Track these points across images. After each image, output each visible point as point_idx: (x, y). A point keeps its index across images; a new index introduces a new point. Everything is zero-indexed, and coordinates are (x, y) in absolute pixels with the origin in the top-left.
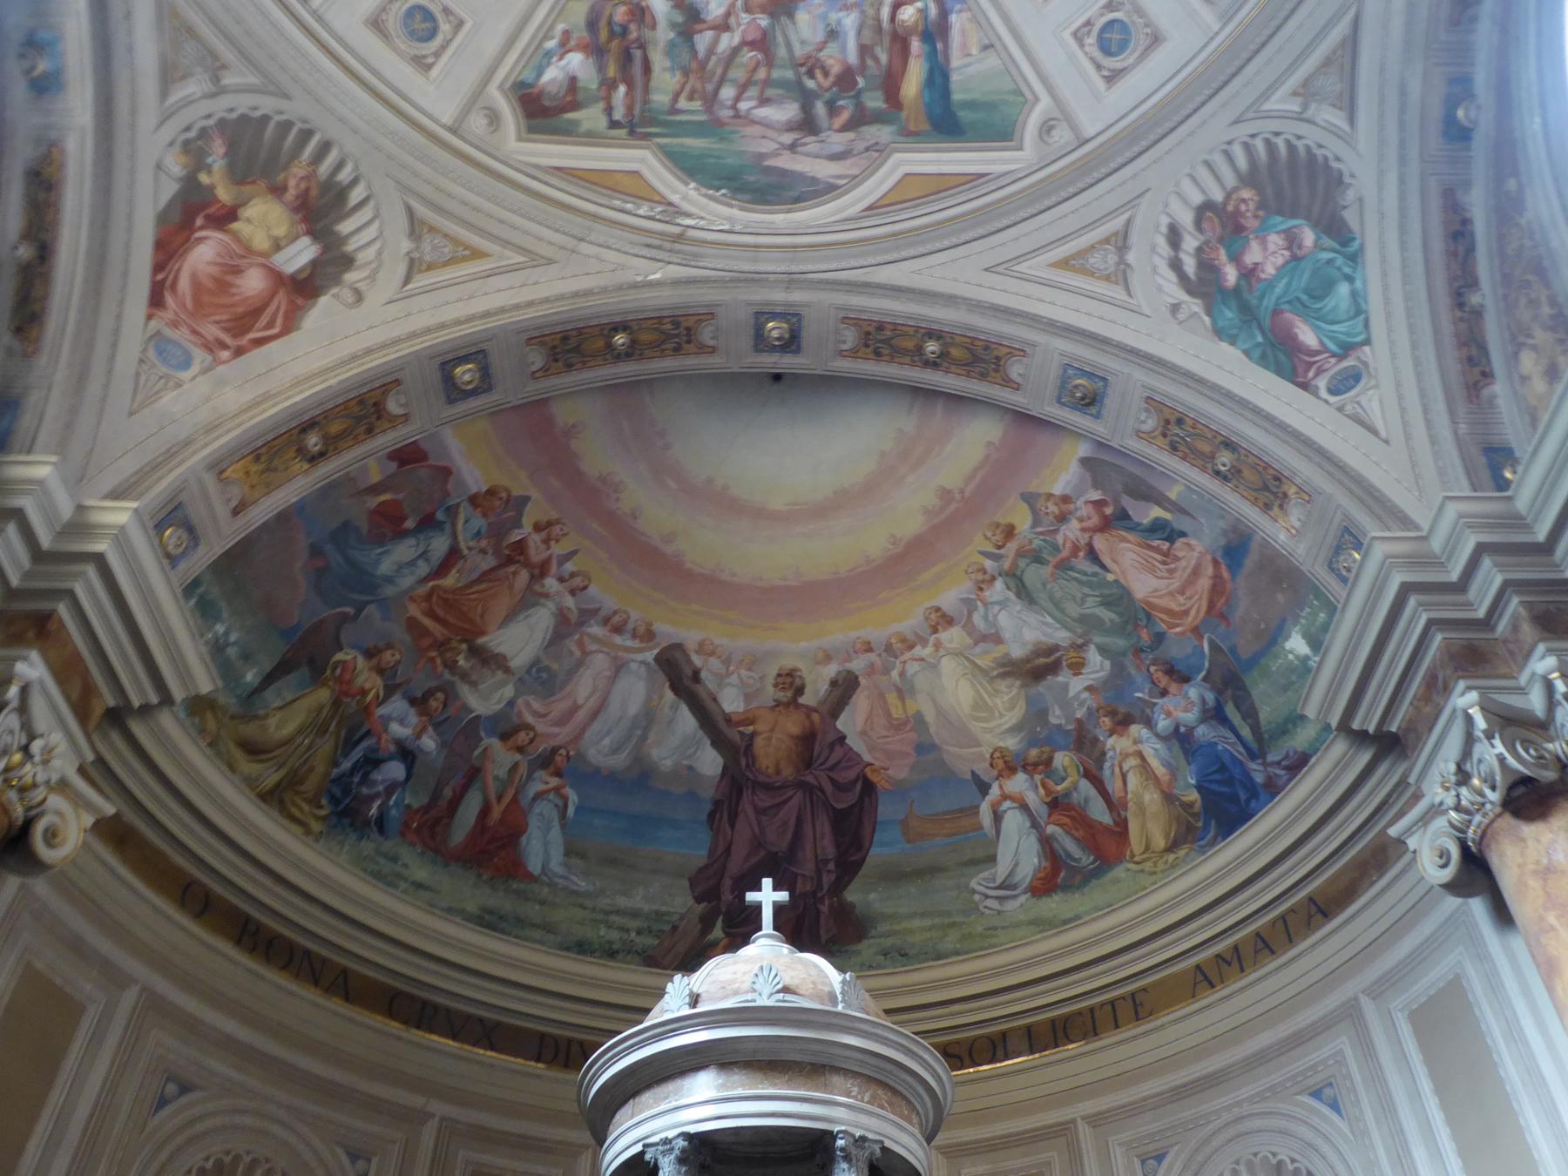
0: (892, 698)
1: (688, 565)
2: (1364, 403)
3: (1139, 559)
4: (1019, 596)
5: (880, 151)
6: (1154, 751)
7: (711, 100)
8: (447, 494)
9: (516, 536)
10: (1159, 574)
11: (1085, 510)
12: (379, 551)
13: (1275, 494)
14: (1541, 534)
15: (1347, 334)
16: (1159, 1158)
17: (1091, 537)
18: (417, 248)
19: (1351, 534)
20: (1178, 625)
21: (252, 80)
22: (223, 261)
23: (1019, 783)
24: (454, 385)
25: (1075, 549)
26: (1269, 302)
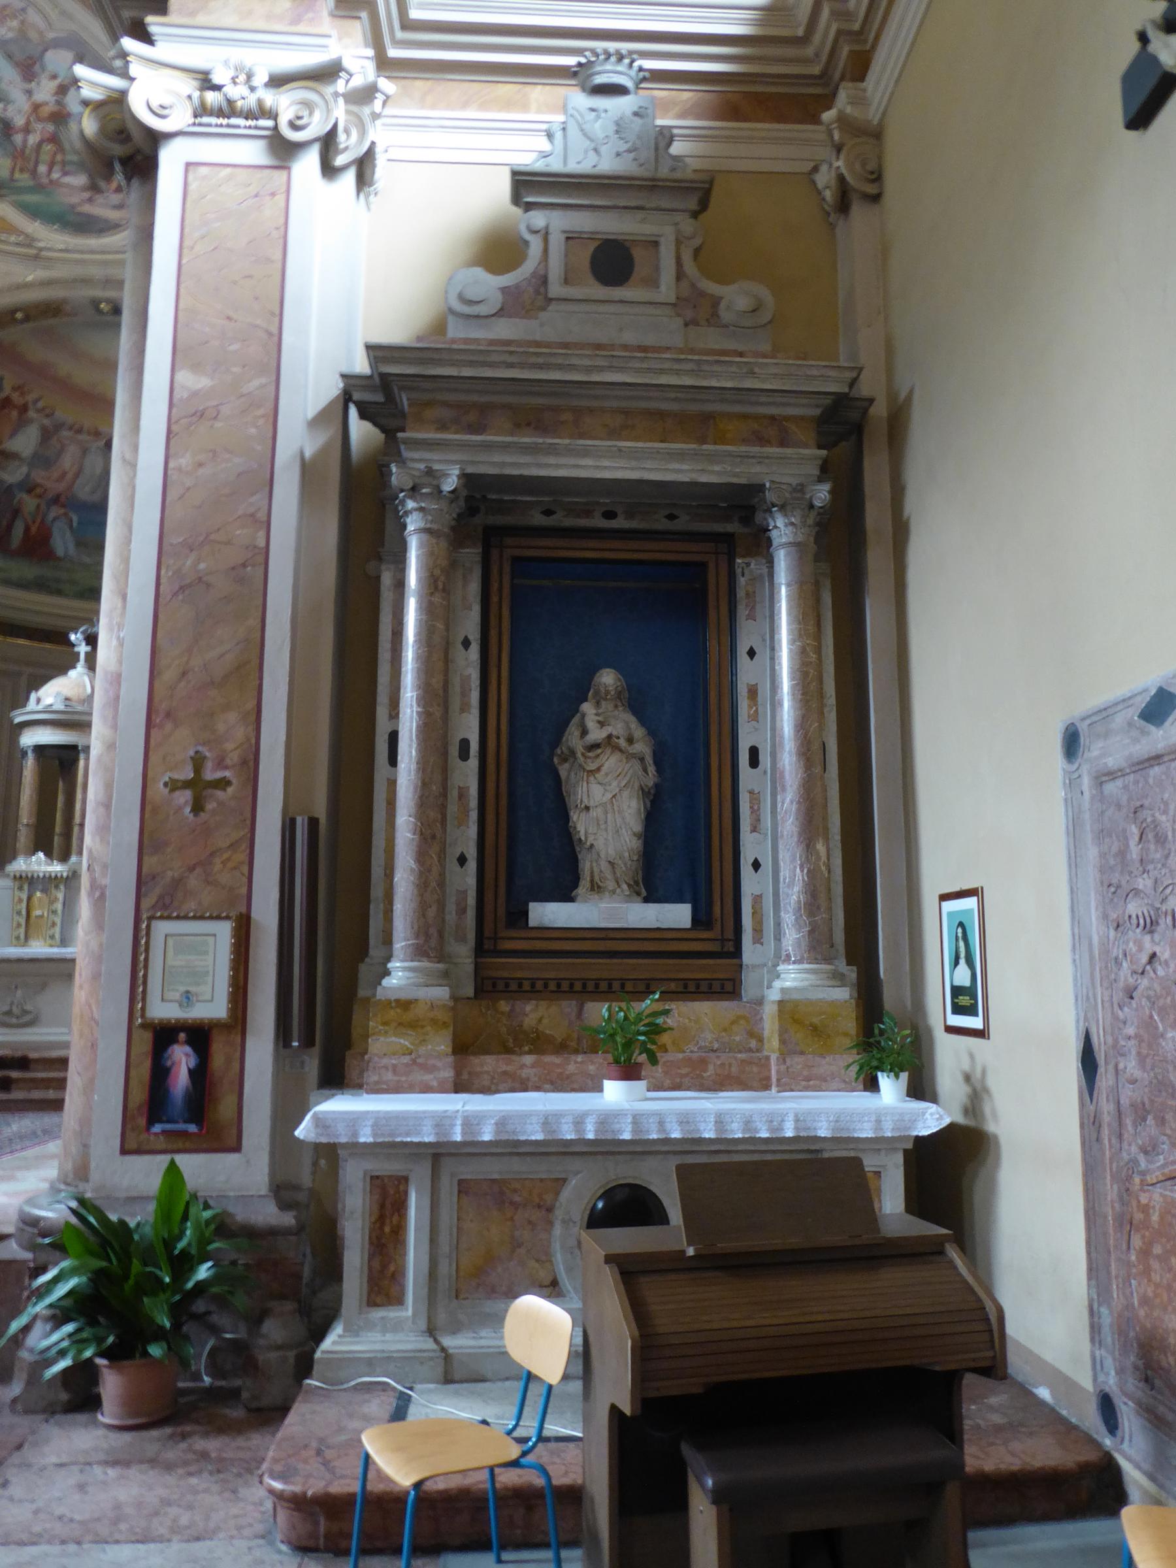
7: (34, 173)
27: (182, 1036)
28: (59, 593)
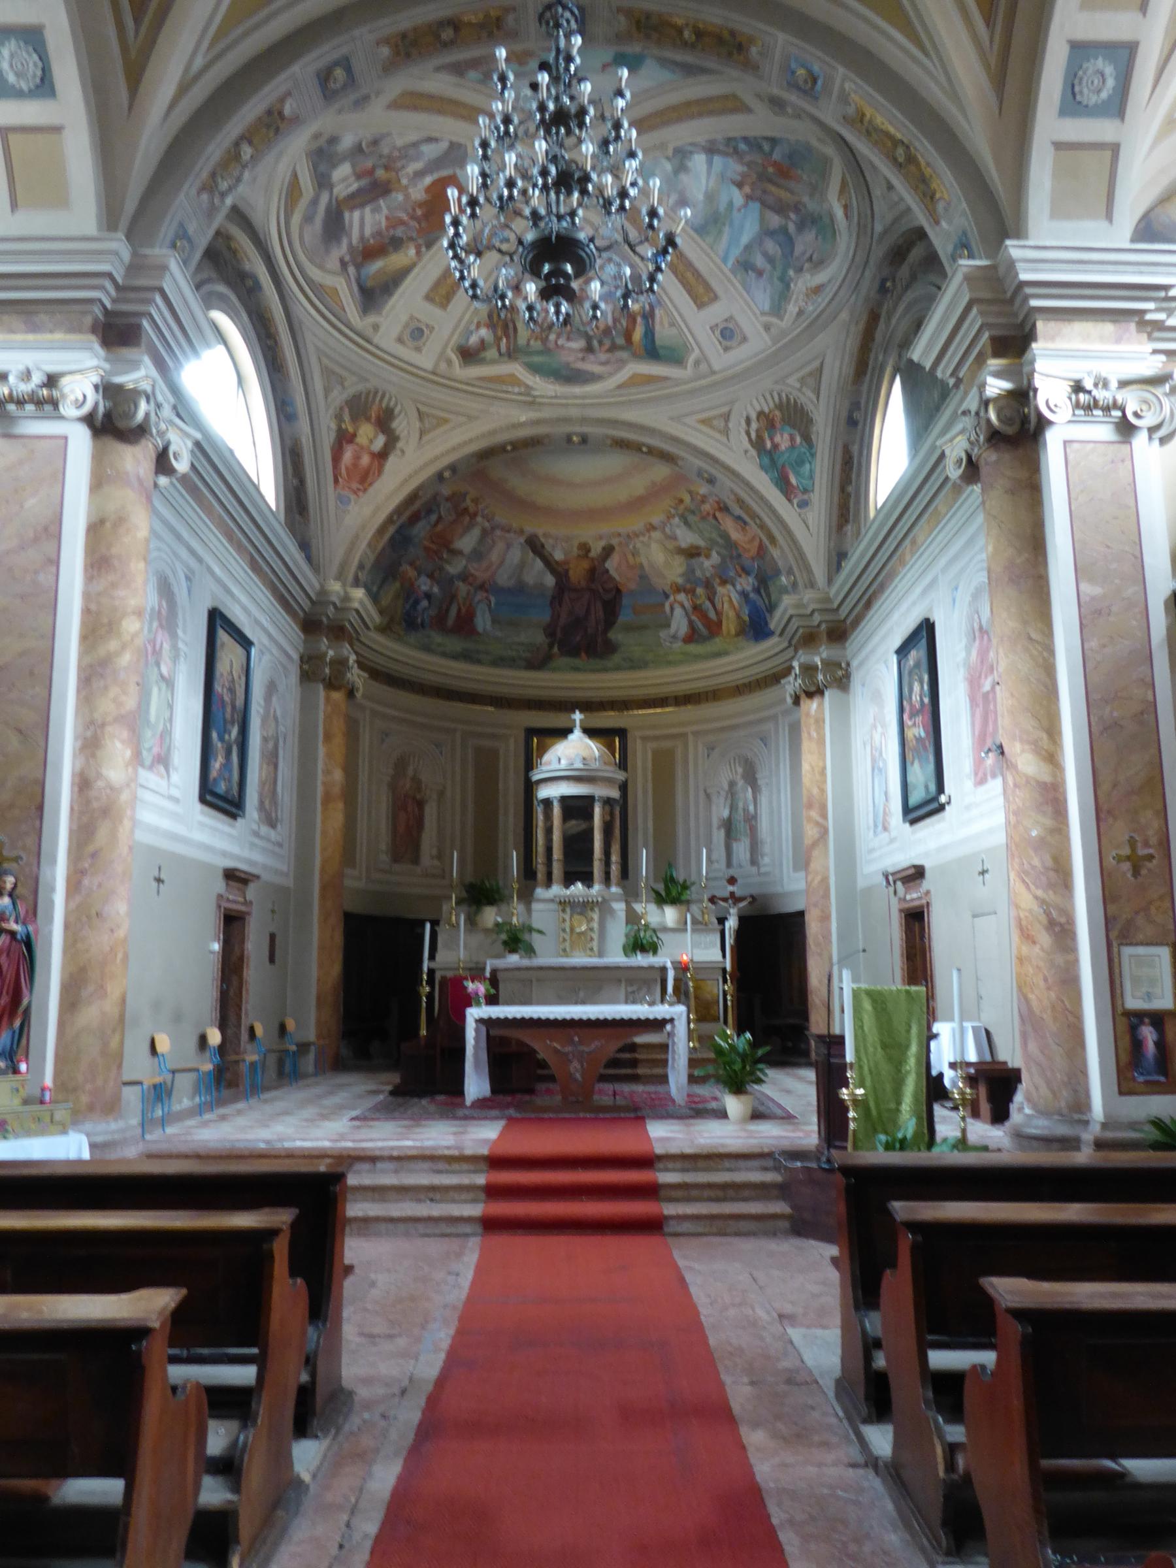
0: (630, 557)
5: (622, 363)
6: (735, 597)
7: (545, 341)
14: (835, 605)
16: (713, 749)
23: (682, 597)
27: (1147, 1020)
28: (479, 662)
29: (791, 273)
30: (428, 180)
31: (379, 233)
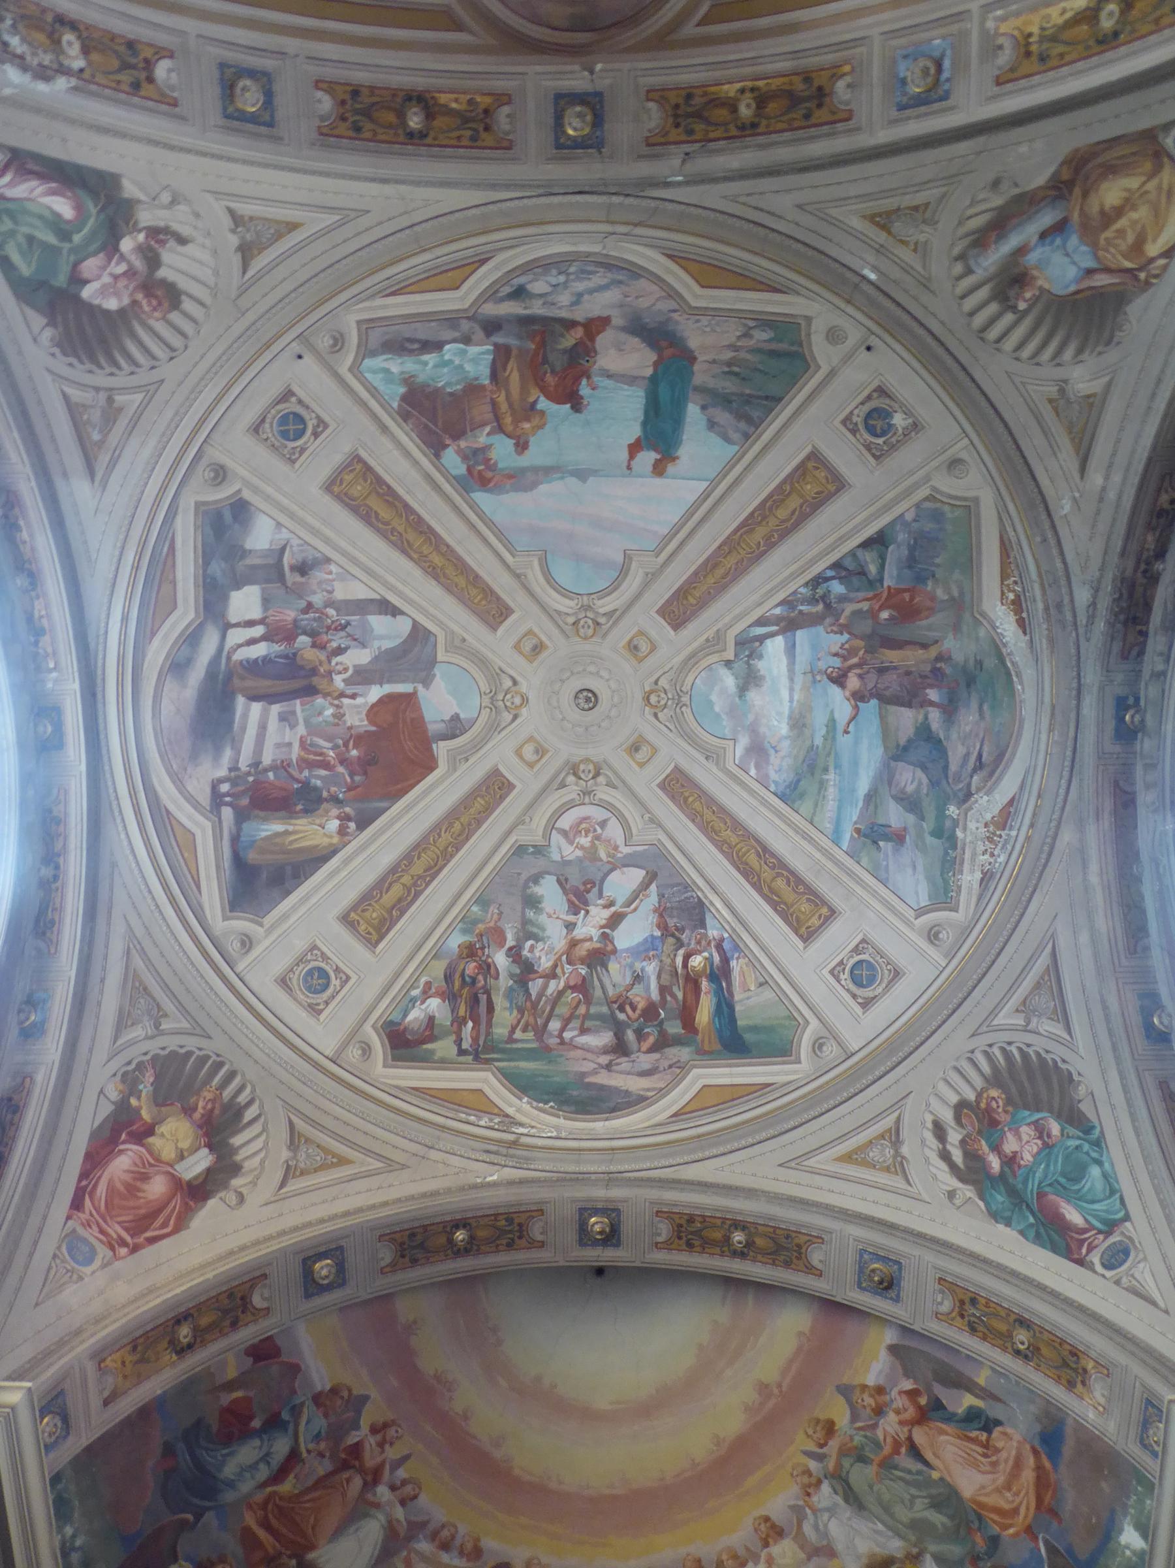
1: (517, 1472)
2: (1137, 1275)
3: (960, 1453)
4: (846, 1500)
5: (682, 1068)
8: (294, 1392)
9: (353, 1438)
10: (983, 1468)
11: (900, 1402)
12: (224, 1452)
13: (1075, 1370)
15: (1107, 1211)
17: (910, 1431)
18: (295, 1157)
19: (1154, 1406)
20: (1011, 1526)
21: (185, 1024)
22: (136, 1169)
24: (313, 1280)
25: (897, 1445)
26: (1032, 1186)
29: (952, 810)
30: (375, 693)
31: (282, 766)
